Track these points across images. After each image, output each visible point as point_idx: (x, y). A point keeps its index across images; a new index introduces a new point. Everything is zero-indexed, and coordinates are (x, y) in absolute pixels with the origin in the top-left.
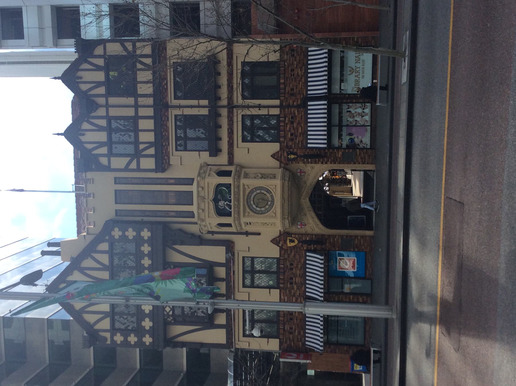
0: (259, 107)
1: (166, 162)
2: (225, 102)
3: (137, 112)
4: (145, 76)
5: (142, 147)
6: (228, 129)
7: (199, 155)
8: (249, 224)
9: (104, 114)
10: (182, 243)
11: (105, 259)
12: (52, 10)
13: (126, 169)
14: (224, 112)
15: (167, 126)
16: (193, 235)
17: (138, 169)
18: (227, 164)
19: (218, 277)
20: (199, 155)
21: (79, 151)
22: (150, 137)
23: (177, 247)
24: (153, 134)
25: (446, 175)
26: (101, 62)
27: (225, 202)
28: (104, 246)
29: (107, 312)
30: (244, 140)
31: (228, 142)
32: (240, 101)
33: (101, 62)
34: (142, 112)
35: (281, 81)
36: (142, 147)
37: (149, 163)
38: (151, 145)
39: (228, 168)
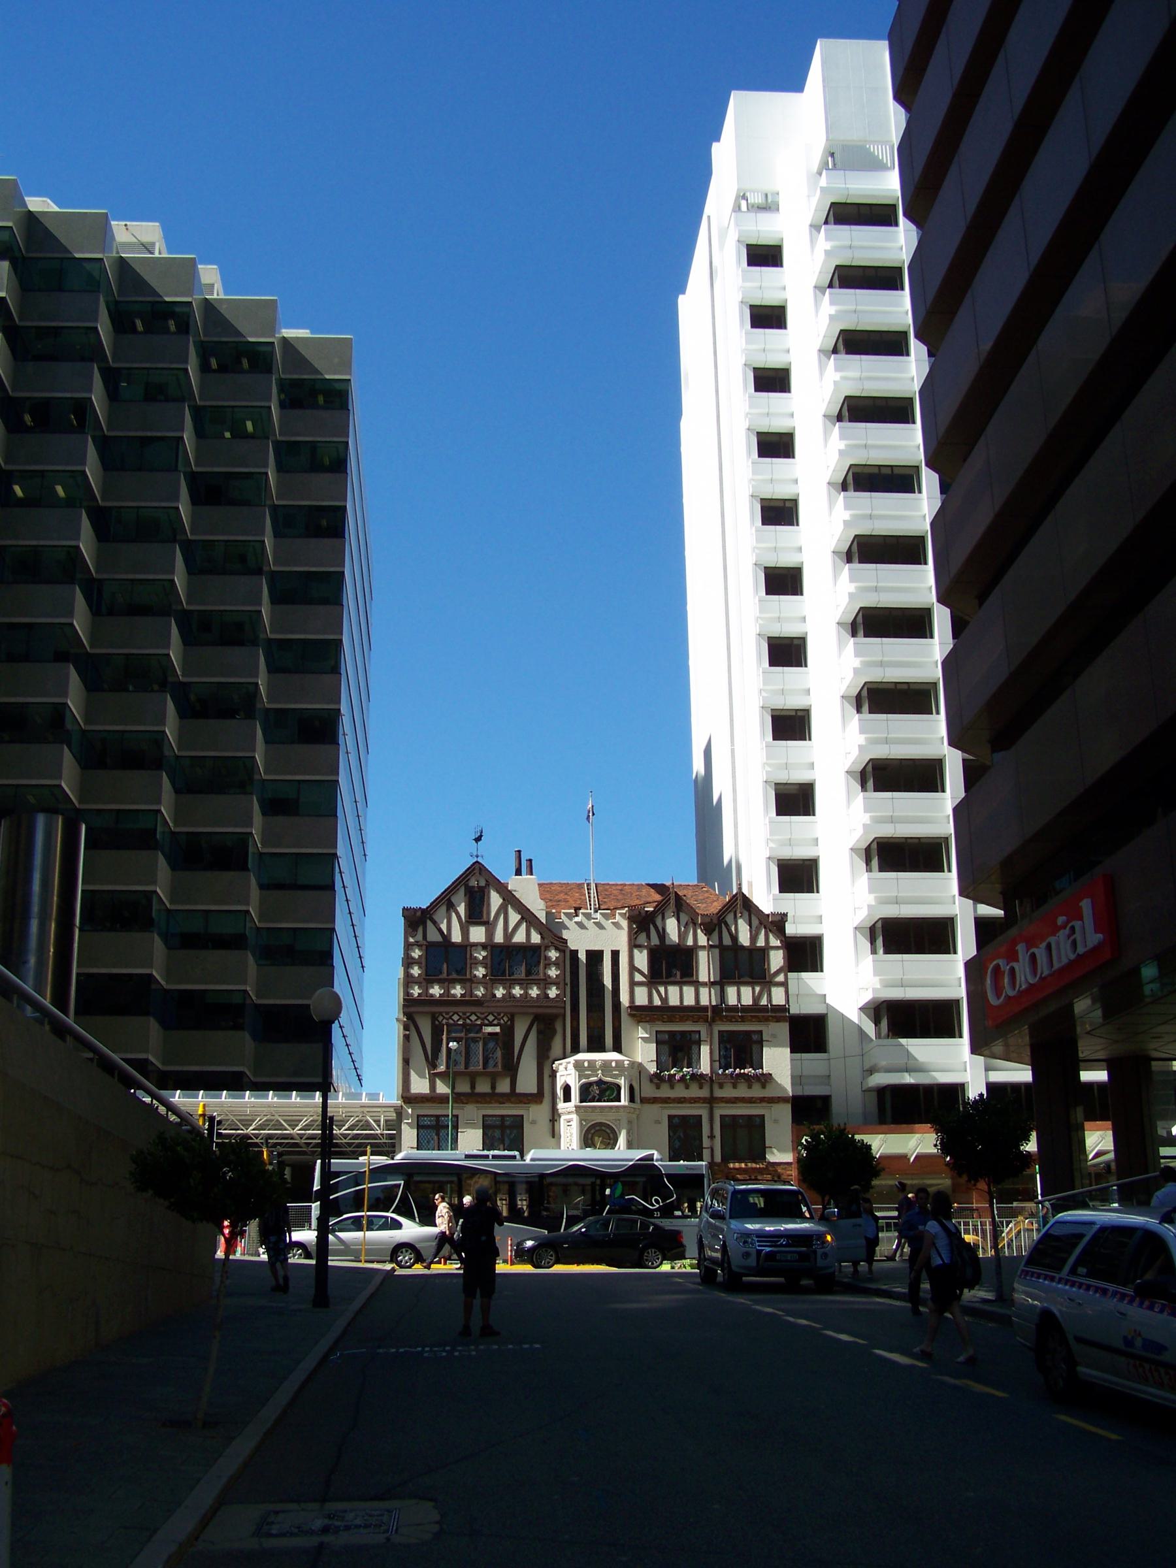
0: (712, 1137)
1: (642, 1018)
2: (719, 1093)
3: (704, 984)
4: (747, 996)
5: (662, 989)
6: (685, 1098)
7: (652, 1061)
8: (569, 1124)
9: (700, 944)
10: (539, 1032)
11: (520, 937)
12: (820, 934)
13: (633, 969)
14: (704, 1093)
15: (686, 1020)
16: (549, 1048)
17: (633, 984)
18: (642, 1096)
19: (497, 1084)
20: (652, 1061)
21: (652, 909)
22: (674, 1001)
23: (534, 1028)
24: (678, 1003)
25: (879, 1207)
26: (761, 942)
27: (598, 1094)
28: (536, 938)
29: (451, 938)
30: (670, 1117)
31: (669, 1098)
32: (718, 1113)
33: (761, 942)
34: (704, 991)
35: (922, 1286)
36: (662, 989)
37: (641, 997)
38: (665, 1000)
39: (637, 1099)
